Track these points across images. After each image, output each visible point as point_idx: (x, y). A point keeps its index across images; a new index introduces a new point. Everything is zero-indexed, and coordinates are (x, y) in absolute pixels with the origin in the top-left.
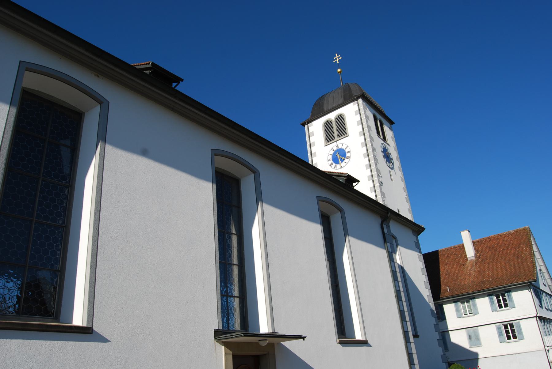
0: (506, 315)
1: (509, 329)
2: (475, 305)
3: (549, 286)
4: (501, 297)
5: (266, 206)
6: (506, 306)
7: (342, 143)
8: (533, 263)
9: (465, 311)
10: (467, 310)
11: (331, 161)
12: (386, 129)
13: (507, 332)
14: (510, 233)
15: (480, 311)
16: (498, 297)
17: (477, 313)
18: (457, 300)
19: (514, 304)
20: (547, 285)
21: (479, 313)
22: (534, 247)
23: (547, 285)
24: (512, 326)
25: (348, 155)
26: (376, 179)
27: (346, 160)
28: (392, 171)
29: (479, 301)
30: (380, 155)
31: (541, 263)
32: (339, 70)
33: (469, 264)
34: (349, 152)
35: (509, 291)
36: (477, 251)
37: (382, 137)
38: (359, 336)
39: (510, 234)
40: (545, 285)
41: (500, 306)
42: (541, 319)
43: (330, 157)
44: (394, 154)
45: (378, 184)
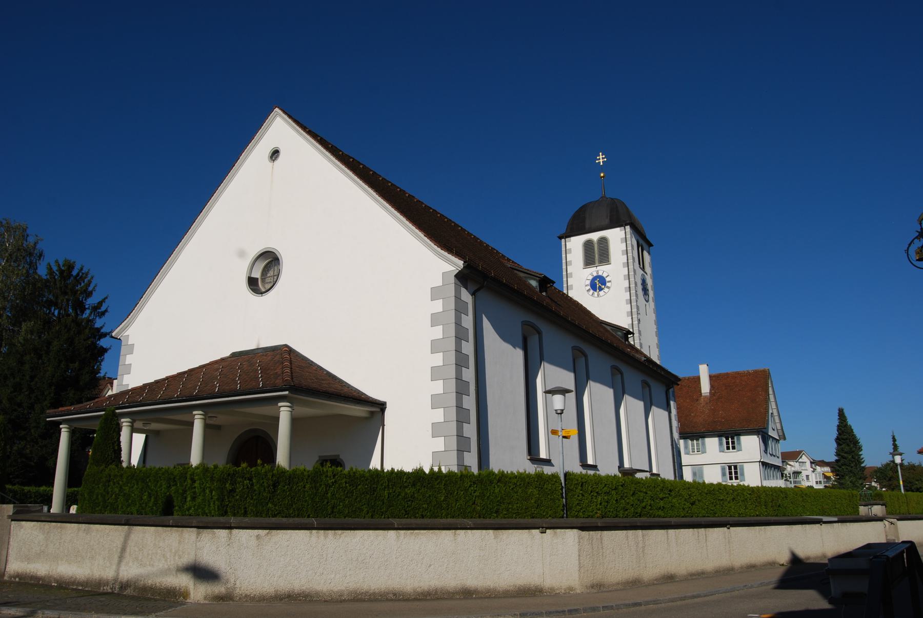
0: (732, 457)
1: (733, 471)
2: (703, 444)
3: (777, 430)
4: (730, 439)
5: (591, 382)
6: (734, 448)
7: (603, 270)
8: (766, 409)
9: (693, 449)
10: (696, 448)
11: (589, 287)
12: (645, 253)
13: (730, 473)
14: (749, 372)
15: (707, 450)
16: (727, 439)
17: (704, 452)
19: (741, 448)
20: (776, 429)
21: (707, 452)
22: (770, 389)
23: (776, 429)
24: (736, 467)
25: (608, 284)
26: (635, 316)
27: (606, 290)
28: (647, 304)
29: (708, 441)
30: (640, 287)
31: (774, 406)
32: (602, 175)
33: (702, 400)
34: (610, 281)
35: (739, 435)
36: (712, 387)
37: (641, 266)
38: (543, 455)
39: (749, 374)
40: (774, 430)
41: (728, 448)
42: (764, 464)
43: (588, 282)
44: (650, 286)
45: (637, 322)
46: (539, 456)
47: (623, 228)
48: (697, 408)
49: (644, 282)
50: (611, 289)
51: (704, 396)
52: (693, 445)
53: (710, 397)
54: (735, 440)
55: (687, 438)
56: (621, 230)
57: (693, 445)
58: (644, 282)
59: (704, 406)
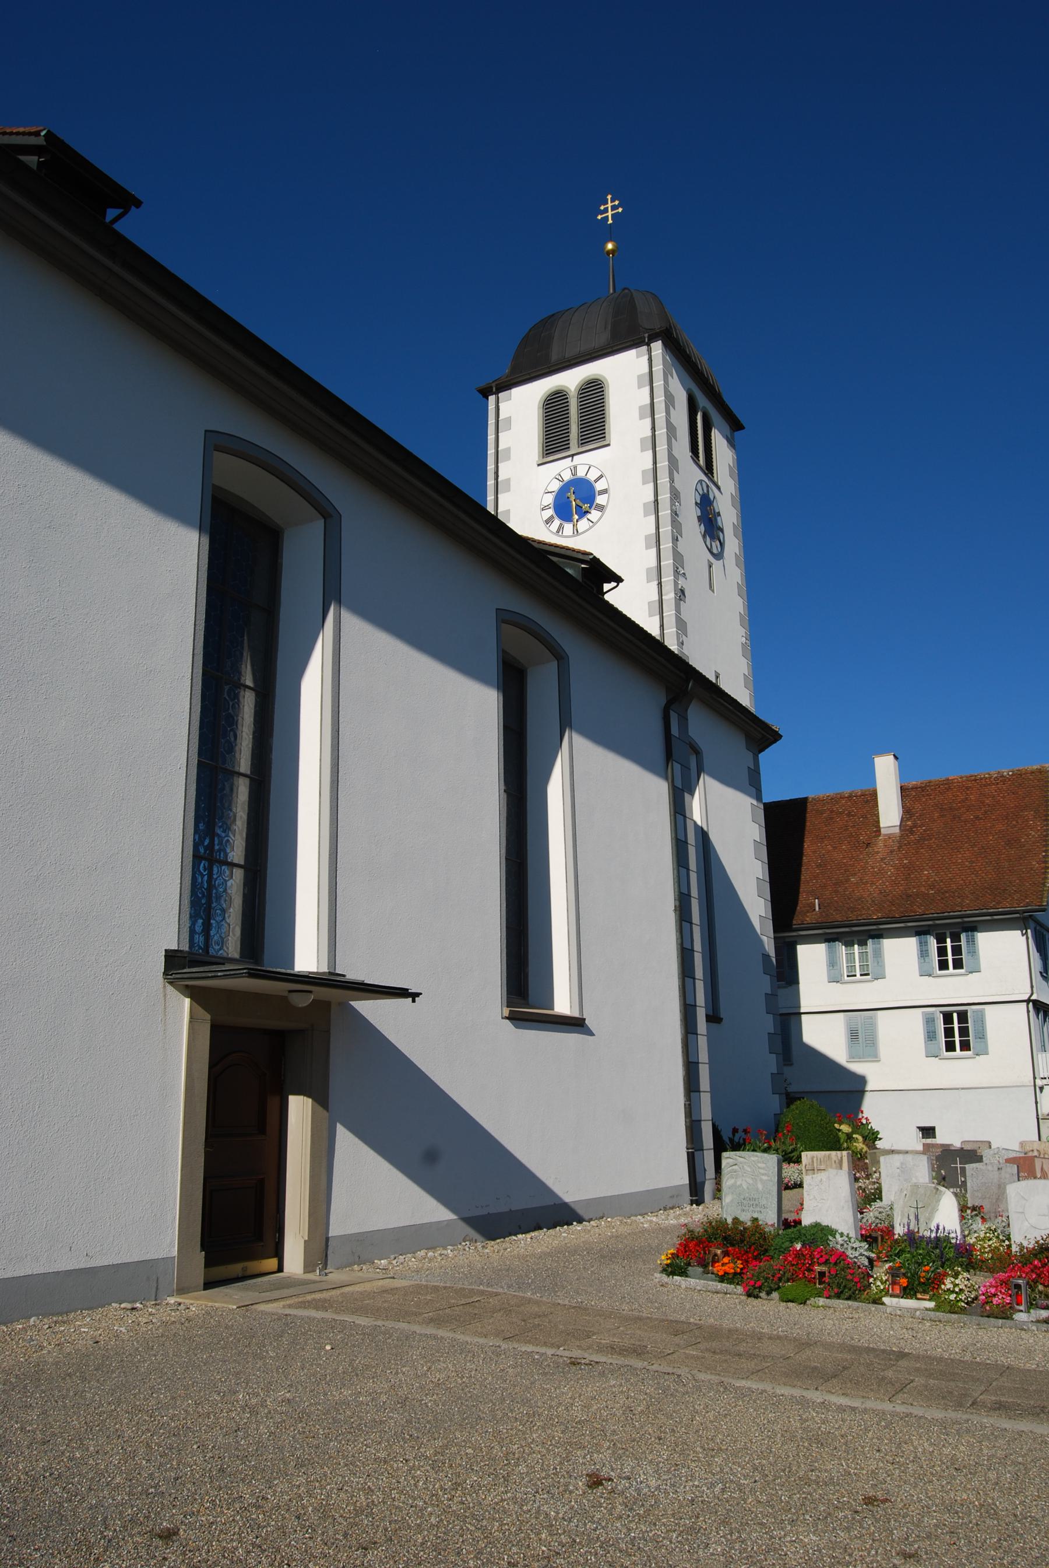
1: (956, 1025)
2: (878, 954)
4: (948, 940)
10: (857, 964)
11: (550, 512)
12: (719, 440)
13: (949, 1032)
14: (1003, 776)
15: (889, 970)
16: (941, 940)
17: (882, 976)
18: (835, 936)
24: (963, 1017)
25: (600, 500)
26: (668, 579)
27: (594, 515)
28: (717, 565)
30: (690, 514)
33: (881, 844)
34: (605, 491)
36: (907, 812)
38: (563, 1004)
39: (1002, 779)
43: (549, 499)
44: (728, 515)
45: (672, 595)
46: (292, 964)
47: (645, 348)
48: (867, 863)
49: (705, 503)
50: (608, 511)
51: (885, 835)
52: (850, 957)
53: (902, 836)
54: (963, 942)
55: (834, 940)
56: (638, 357)
57: (850, 957)
58: (705, 503)
59: (882, 859)
